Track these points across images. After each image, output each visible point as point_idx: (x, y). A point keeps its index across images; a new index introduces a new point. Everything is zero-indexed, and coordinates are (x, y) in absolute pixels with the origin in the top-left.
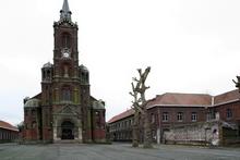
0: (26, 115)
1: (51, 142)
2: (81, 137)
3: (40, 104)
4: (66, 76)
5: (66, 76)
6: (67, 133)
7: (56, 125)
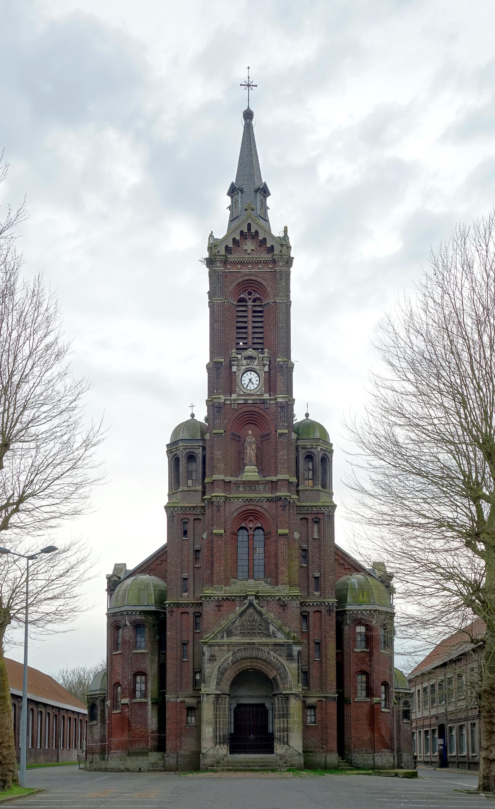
0: (114, 643)
1: (195, 764)
2: (296, 742)
3: (161, 598)
4: (251, 473)
5: (251, 473)
6: (251, 734)
7: (210, 688)
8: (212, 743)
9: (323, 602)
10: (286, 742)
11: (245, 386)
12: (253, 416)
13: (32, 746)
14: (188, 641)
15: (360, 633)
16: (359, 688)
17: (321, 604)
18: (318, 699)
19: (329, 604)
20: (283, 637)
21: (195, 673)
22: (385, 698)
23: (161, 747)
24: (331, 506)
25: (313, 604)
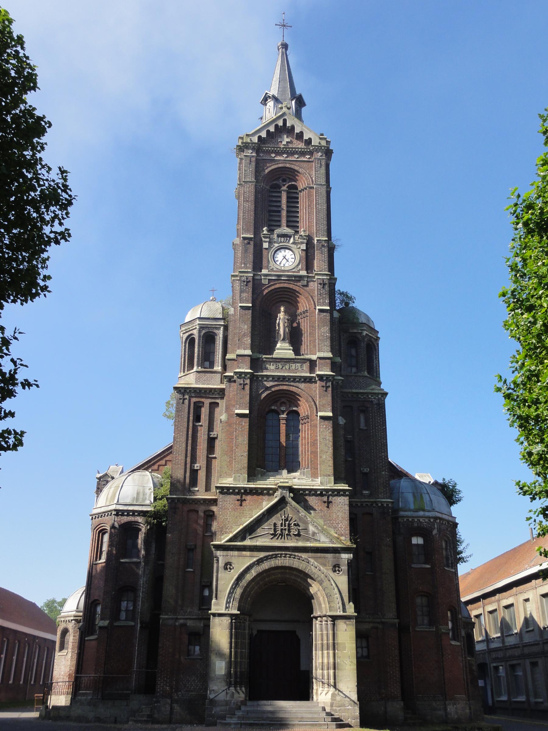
8: (224, 684)
9: (375, 502)
10: (332, 684)
11: (278, 263)
12: (286, 293)
13: (35, 681)
14: (195, 546)
15: (418, 545)
16: (419, 613)
17: (372, 505)
18: (371, 625)
19: (382, 505)
20: (327, 540)
21: (203, 587)
22: (453, 627)
23: (148, 688)
24: (381, 393)
25: (362, 505)
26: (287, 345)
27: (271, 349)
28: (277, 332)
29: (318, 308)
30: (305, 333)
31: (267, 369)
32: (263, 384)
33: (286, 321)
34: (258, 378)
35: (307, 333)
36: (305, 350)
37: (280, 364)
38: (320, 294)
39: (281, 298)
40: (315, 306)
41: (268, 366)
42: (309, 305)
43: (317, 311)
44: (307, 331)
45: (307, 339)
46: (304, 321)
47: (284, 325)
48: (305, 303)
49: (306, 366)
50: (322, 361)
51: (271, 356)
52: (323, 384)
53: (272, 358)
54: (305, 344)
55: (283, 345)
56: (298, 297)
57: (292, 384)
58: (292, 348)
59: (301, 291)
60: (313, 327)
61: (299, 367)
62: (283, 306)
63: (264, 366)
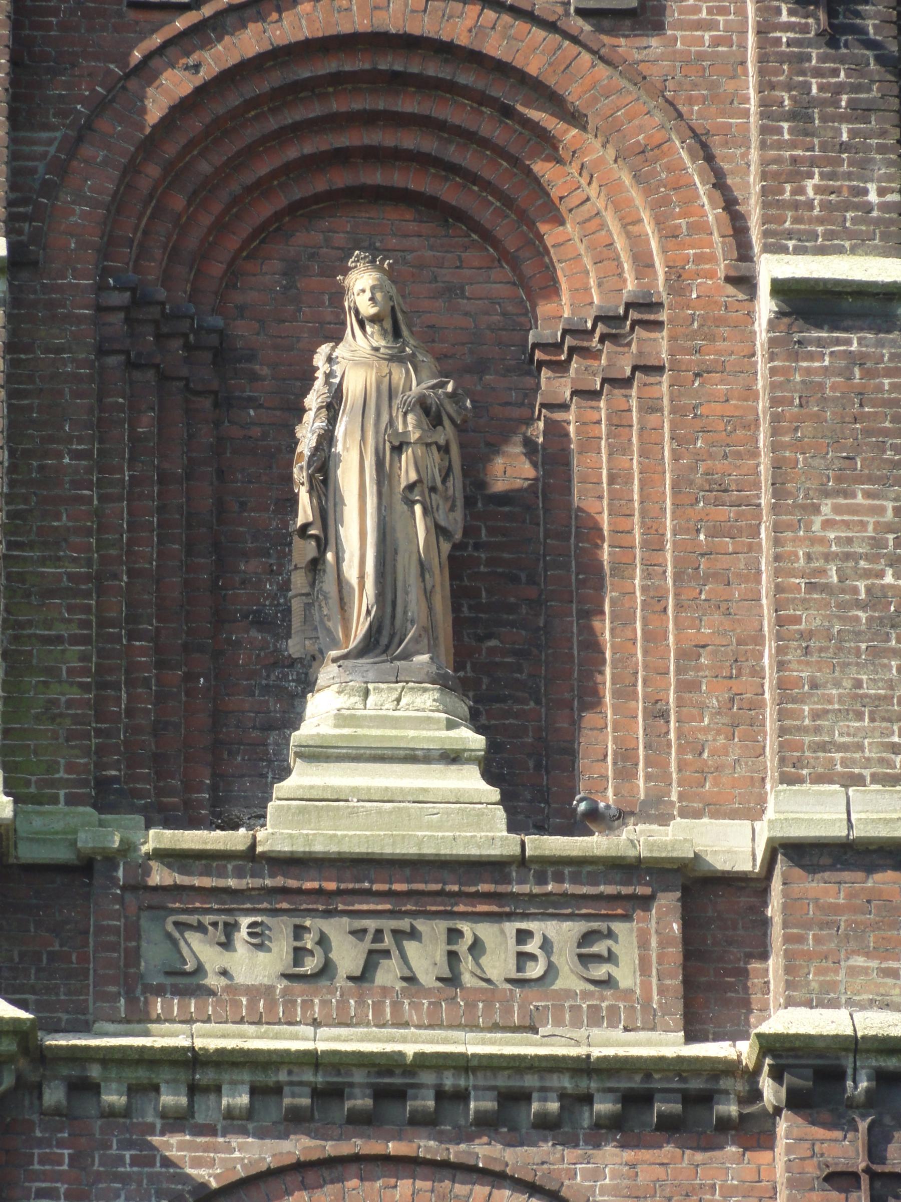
12: (409, 105)
26: (424, 701)
27: (227, 746)
28: (304, 550)
29: (771, 268)
30: (622, 569)
31: (187, 983)
32: (148, 1156)
33: (410, 426)
34: (83, 1088)
35: (652, 568)
36: (626, 756)
37: (336, 930)
38: (800, 115)
39: (341, 157)
40: (744, 254)
41: (201, 949)
42: (669, 235)
43: (766, 306)
44: (654, 544)
45: (654, 638)
46: (619, 422)
47: (384, 475)
48: (629, 223)
49: (644, 947)
50: (827, 889)
51: (235, 840)
52: (847, 1149)
53: (250, 856)
54: (625, 693)
55: (381, 700)
56: (547, 144)
57: (484, 1151)
58: (476, 741)
59: (582, 77)
60: (718, 490)
61: (565, 960)
62: (374, 253)
63: (153, 955)
